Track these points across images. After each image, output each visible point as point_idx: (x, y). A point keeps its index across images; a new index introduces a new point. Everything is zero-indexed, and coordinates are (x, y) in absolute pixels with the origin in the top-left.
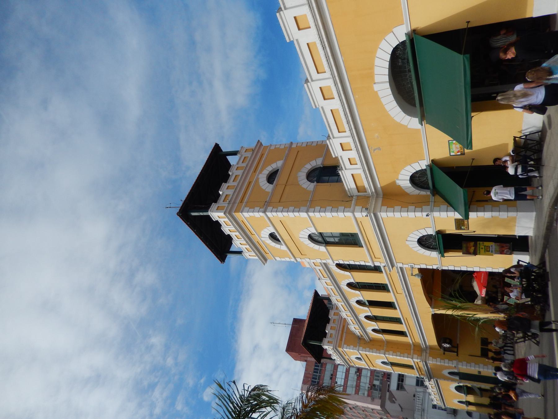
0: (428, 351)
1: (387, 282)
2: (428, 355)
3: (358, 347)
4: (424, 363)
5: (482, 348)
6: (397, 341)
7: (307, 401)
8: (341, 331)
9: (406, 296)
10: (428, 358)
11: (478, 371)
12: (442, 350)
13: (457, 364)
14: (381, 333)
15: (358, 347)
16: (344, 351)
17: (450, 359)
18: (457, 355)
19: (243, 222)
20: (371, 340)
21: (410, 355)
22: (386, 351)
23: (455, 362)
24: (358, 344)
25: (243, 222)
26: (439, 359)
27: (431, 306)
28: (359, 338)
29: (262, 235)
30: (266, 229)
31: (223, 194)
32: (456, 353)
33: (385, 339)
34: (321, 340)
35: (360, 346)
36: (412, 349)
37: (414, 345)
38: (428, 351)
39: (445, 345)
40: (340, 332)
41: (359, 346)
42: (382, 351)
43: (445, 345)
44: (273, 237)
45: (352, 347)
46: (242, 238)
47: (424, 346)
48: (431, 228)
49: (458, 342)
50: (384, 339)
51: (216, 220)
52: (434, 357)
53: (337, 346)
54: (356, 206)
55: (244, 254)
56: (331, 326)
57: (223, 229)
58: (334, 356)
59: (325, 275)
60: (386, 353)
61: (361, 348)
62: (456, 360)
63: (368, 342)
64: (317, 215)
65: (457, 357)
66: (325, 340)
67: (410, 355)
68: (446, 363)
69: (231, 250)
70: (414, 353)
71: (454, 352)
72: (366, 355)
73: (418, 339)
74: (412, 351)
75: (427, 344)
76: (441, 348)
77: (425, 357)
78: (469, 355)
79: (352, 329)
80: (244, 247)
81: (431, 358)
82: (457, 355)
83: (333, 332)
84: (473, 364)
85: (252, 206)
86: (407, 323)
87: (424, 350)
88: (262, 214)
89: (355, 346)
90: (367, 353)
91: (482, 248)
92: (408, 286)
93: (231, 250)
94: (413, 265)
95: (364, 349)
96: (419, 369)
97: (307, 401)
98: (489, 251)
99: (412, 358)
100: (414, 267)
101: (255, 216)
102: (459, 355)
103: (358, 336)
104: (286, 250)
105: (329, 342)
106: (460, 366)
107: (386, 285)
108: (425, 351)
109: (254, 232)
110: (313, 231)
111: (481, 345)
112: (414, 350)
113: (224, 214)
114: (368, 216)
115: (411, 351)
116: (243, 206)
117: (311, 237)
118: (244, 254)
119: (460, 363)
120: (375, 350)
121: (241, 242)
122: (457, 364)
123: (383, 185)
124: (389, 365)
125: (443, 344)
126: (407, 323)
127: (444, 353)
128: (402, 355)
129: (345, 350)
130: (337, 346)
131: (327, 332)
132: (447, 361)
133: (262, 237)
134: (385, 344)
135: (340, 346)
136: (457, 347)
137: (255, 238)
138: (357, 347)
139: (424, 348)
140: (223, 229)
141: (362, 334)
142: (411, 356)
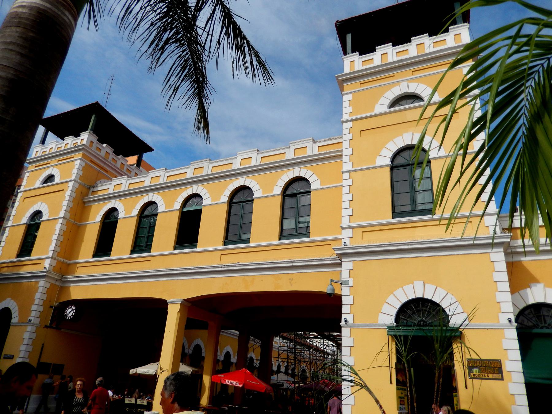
0: (58, 283)
1: (153, 252)
2: (53, 282)
3: (80, 181)
4: (45, 274)
5: (51, 364)
6: (82, 241)
7: (73, 13)
8: (103, 166)
9: (312, 261)
10: (49, 281)
11: (13, 356)
12: (57, 304)
13: (33, 325)
14: (103, 220)
15: (80, 181)
16: (75, 160)
17: (42, 315)
18: (46, 327)
19: (392, 76)
20: (84, 203)
21: (518, 212)
22: (67, 221)
23: (37, 321)
24: (83, 183)
25: (392, 76)
26: (45, 297)
27: (184, 300)
28: (89, 188)
29: (55, 169)
30: (344, 97)
31: (103, 147)
32: (49, 325)
33: (86, 224)
34: (95, 131)
35: (79, 186)
36: (65, 260)
37: (69, 265)
38: (58, 283)
39: (72, 310)
40: (102, 164)
41: (80, 184)
42: (68, 216)
43: (70, 310)
44: (50, 178)
45: (81, 173)
46: (58, 150)
47: (69, 279)
48: (353, 323)
49: (62, 330)
50: (87, 223)
51: (81, 135)
52: (49, 291)
53: (86, 153)
54: (57, 261)
55: (41, 146)
56: (109, 154)
57: (71, 137)
58: (56, 145)
59: (132, 187)
60: (65, 221)
61: (77, 185)
62: (39, 323)
63: (82, 199)
64: (58, 226)
65: (44, 326)
66: (95, 139)
67: (57, 256)
68: (35, 309)
69: (49, 132)
70: (58, 261)
71: (51, 324)
72: (63, 190)
73: (81, 273)
74: (62, 259)
75: (72, 285)
76: (59, 303)
77: (51, 277)
78: (43, 344)
79: (151, 173)
80: (48, 150)
81: (48, 285)
82: (46, 327)
83: (103, 153)
84: (30, 349)
85: (85, 169)
86: (92, 264)
87: (62, 278)
88: (73, 177)
89: (81, 178)
90: (68, 193)
91: (402, 393)
92: (158, 278)
93: (49, 132)
94: (351, 285)
95: (74, 190)
96: (16, 264)
97: (73, 13)
98: (401, 404)
99: (52, 258)
100: (343, 286)
101: (74, 169)
102: (46, 329)
103: (94, 187)
104: (34, 186)
105: (92, 142)
106: (29, 328)
107: (196, 247)
108: (60, 278)
109: (364, 87)
110: (45, 217)
111: (54, 364)
112: (63, 263)
113: (84, 144)
114: (45, 269)
115: (63, 258)
116: (87, 161)
117: (38, 214)
118: (41, 146)
119: (34, 329)
120: (71, 205)
121: (39, 152)
122: (33, 325)
123: (71, 289)
124: (29, 221)
125: (74, 308)
126: (92, 264)
127: (51, 307)
128: (59, 242)
129: (78, 162)
130: (86, 153)
131: (105, 145)
132: (41, 309)
133: (54, 168)
134: (77, 223)
135: (84, 156)
136: (58, 328)
137: (54, 162)
138: (79, 180)
139: (67, 278)
140: (71, 137)
141: (100, 194)
142: (55, 256)
